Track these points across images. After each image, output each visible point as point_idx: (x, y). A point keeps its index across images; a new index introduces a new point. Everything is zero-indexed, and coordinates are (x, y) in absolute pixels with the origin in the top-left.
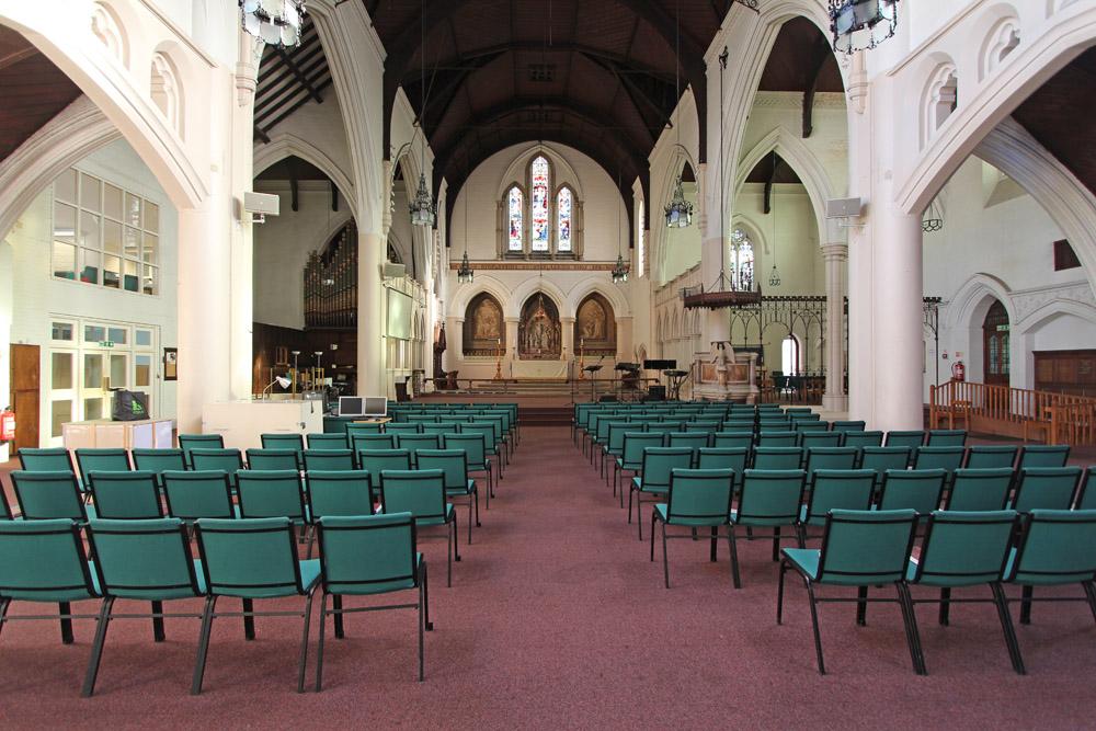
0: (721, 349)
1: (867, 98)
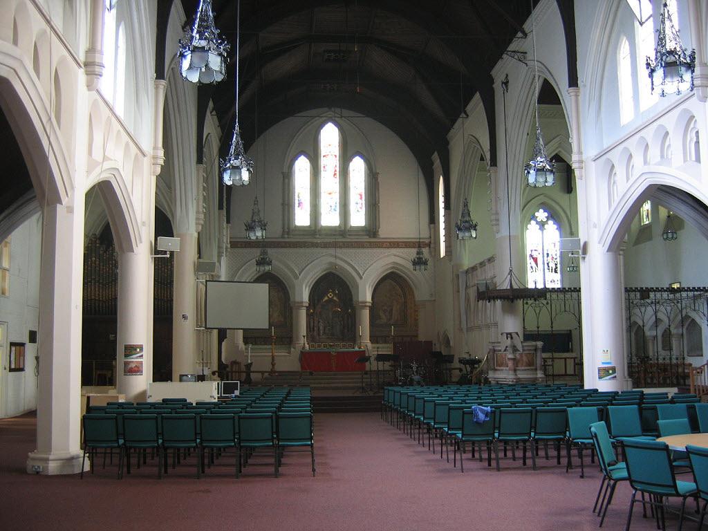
0: (509, 339)
1: (583, 170)
